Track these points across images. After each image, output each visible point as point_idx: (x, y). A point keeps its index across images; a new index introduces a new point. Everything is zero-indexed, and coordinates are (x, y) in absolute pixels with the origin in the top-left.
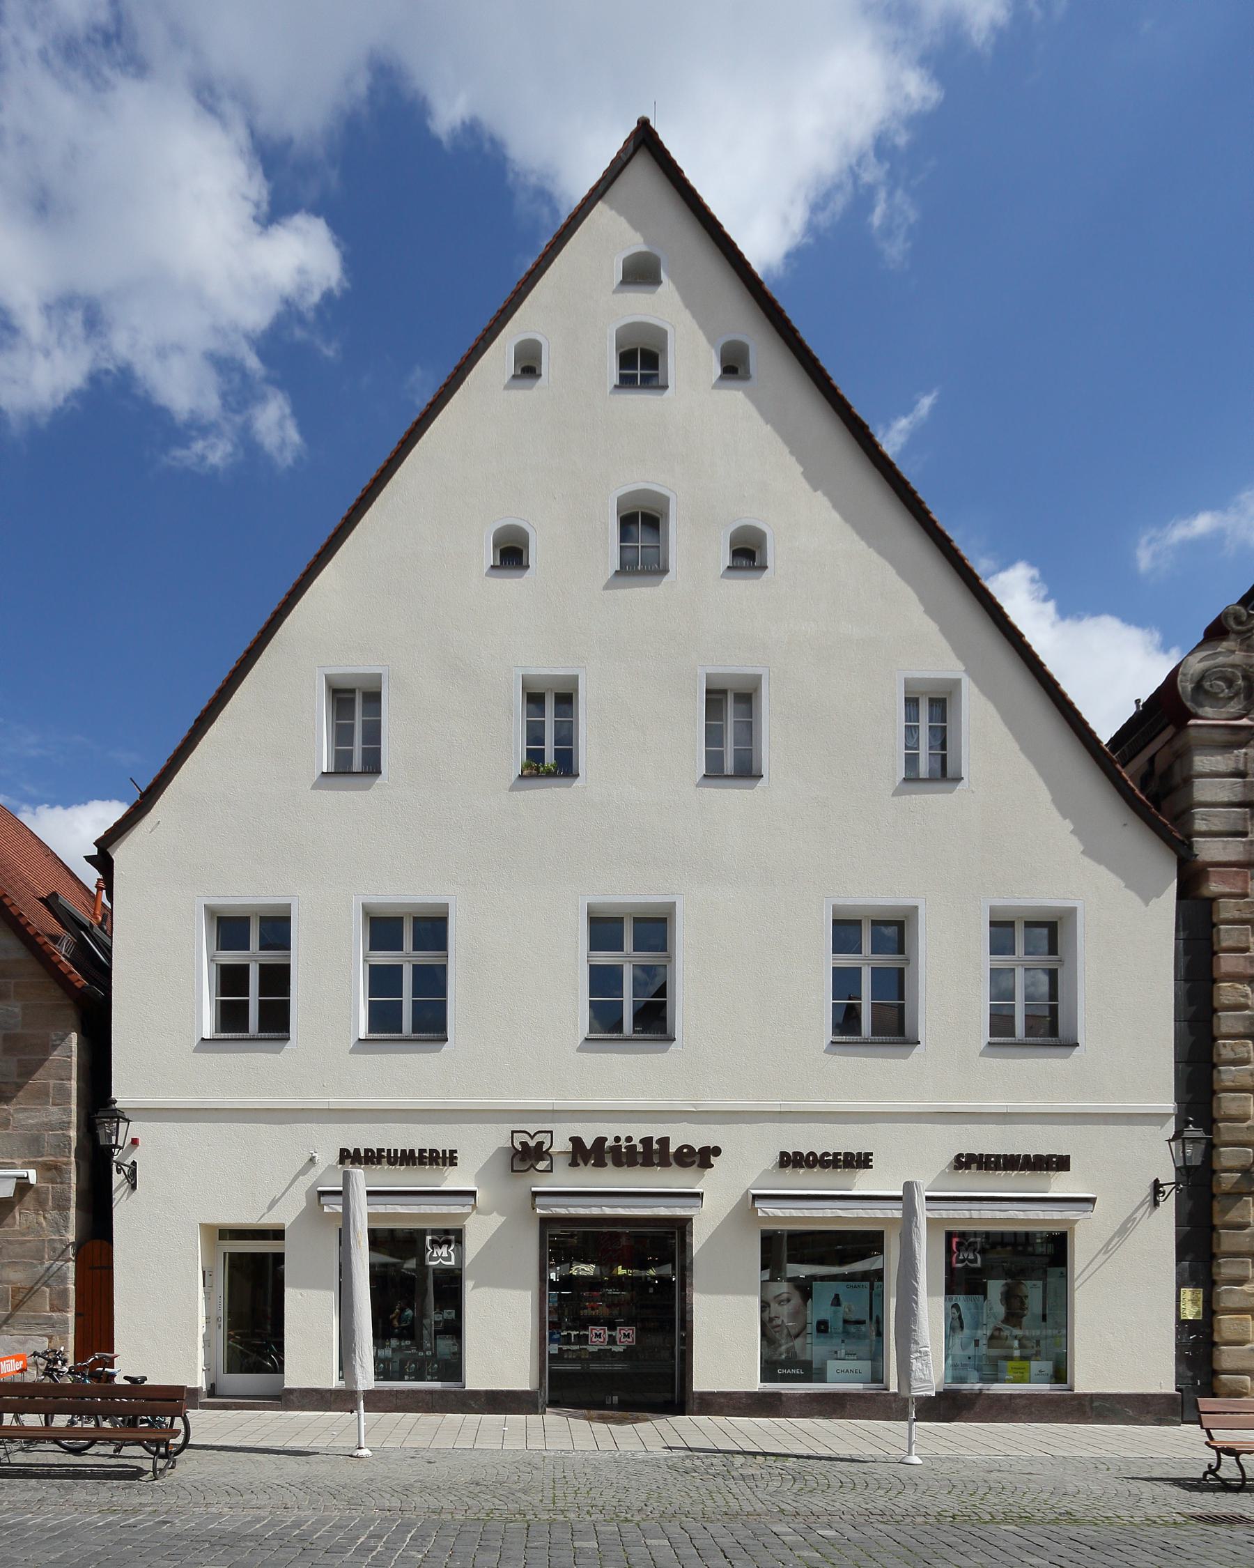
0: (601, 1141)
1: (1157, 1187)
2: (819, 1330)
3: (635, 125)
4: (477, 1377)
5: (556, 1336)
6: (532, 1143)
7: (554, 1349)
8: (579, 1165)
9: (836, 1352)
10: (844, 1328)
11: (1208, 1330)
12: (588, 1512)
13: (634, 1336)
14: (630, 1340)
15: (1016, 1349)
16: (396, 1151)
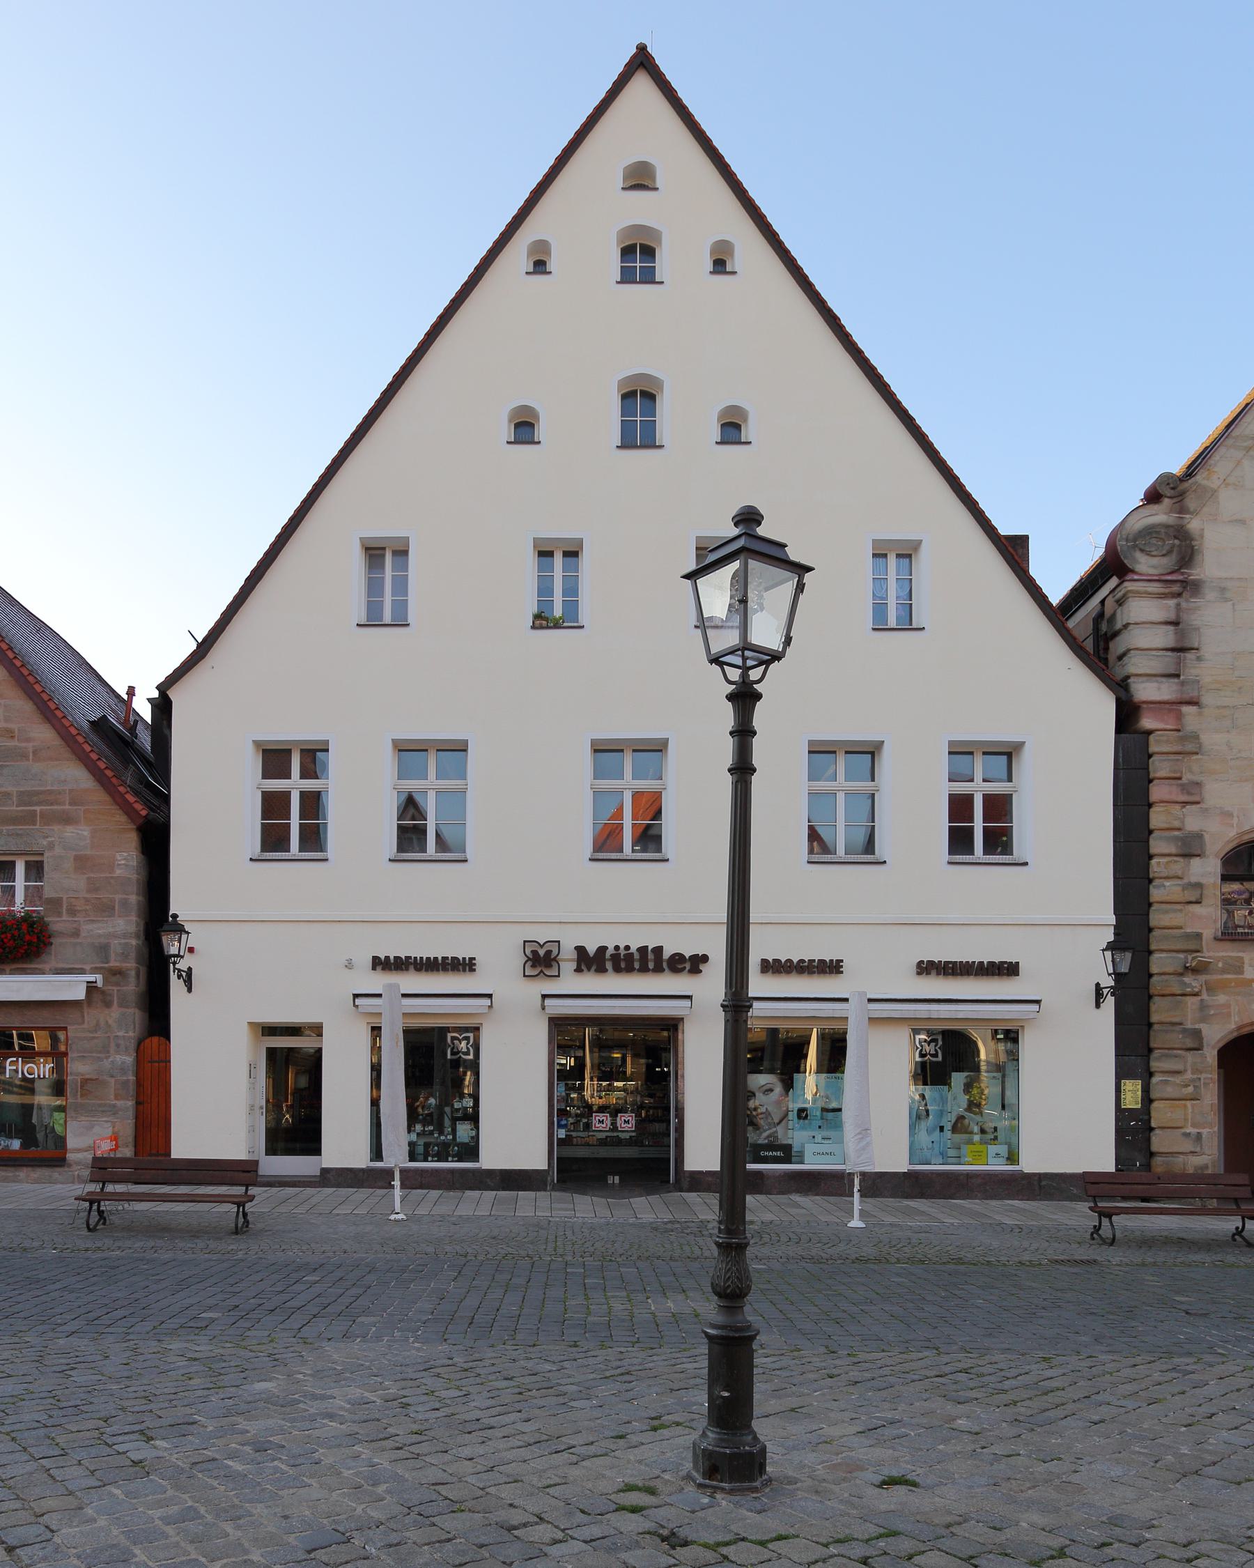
0: (602, 950)
1: (1098, 988)
2: (799, 1117)
3: (634, 50)
4: (491, 1158)
5: (563, 1122)
6: (542, 952)
7: (562, 1134)
8: (583, 971)
9: (814, 1137)
10: (822, 1115)
11: (1146, 1117)
12: (581, 1256)
13: (634, 1122)
14: (630, 1125)
15: (976, 1134)
16: (421, 958)
